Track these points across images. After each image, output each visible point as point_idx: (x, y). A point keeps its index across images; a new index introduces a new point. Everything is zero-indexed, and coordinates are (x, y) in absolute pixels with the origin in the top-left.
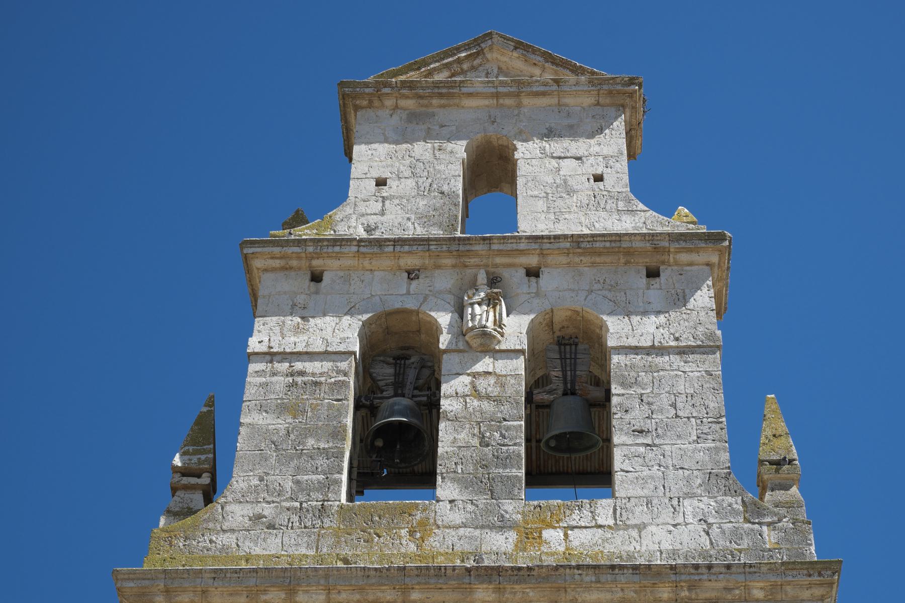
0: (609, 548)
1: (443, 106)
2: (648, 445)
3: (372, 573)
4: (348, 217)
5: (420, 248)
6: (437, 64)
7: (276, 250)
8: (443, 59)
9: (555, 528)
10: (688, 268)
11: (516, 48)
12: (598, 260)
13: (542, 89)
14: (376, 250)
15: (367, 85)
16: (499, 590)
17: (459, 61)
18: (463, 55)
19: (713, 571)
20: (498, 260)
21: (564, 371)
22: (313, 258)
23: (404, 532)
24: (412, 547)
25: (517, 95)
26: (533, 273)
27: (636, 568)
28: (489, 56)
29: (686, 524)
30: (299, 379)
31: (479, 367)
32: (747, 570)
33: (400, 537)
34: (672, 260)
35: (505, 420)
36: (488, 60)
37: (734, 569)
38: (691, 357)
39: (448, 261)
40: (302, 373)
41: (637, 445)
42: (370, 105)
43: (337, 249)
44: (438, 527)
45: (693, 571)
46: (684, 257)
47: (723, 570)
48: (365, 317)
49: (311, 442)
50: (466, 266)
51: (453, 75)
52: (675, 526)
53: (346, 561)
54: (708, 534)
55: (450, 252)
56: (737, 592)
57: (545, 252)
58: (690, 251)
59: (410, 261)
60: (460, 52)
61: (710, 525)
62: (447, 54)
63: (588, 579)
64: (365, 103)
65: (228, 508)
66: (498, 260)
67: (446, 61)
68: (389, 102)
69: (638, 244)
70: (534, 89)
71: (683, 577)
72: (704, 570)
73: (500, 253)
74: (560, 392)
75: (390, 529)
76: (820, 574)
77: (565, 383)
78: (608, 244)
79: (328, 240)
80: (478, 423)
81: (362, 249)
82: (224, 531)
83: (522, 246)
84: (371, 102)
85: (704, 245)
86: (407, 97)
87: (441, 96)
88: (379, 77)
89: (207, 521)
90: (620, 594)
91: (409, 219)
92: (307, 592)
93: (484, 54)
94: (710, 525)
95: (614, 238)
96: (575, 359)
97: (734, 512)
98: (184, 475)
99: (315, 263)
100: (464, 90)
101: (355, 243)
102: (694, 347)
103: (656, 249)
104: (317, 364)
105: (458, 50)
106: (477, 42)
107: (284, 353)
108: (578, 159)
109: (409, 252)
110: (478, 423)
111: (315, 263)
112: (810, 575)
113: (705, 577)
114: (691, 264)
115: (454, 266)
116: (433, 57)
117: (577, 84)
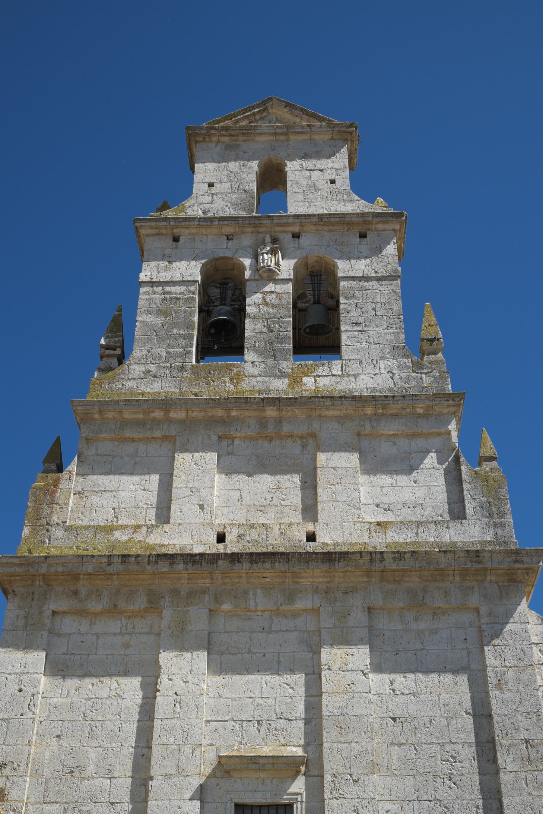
0: (339, 387)
1: (245, 141)
2: (360, 331)
3: (211, 401)
4: (193, 205)
5: (233, 222)
6: (241, 116)
7: (154, 224)
8: (245, 113)
9: (309, 376)
10: (382, 232)
11: (286, 106)
12: (332, 228)
13: (301, 130)
14: (209, 223)
15: (202, 129)
16: (279, 410)
17: (254, 114)
18: (256, 110)
19: (395, 399)
20: (277, 229)
21: (314, 290)
22: (173, 228)
23: (227, 379)
24: (232, 387)
25: (287, 134)
26: (296, 236)
27: (353, 397)
28: (270, 111)
29: (381, 374)
30: (168, 296)
31: (267, 289)
32: (414, 398)
33: (225, 382)
34: (373, 228)
35: (281, 318)
36: (270, 114)
37: (406, 398)
38: (384, 282)
39: (249, 230)
40: (169, 293)
41: (354, 331)
42: (204, 141)
43: (187, 223)
44: (246, 376)
45: (384, 399)
46: (381, 226)
47: (401, 398)
48: (204, 261)
49: (175, 331)
50: (259, 232)
51: (250, 123)
52: (375, 375)
53: (196, 395)
54: (392, 379)
55: (250, 224)
56: (408, 410)
57: (303, 224)
58: (384, 222)
59: (229, 230)
60: (254, 109)
61: (394, 374)
62: (247, 110)
63: (327, 404)
64: (201, 139)
65: (131, 367)
66: (277, 229)
67: (246, 114)
68: (214, 139)
69: (355, 219)
70: (296, 130)
71: (379, 402)
72: (391, 398)
73: (278, 225)
74: (312, 302)
75: (220, 378)
76: (453, 400)
77: (314, 297)
78: (338, 219)
79: (182, 218)
80: (267, 320)
81: (201, 223)
82: (130, 379)
83: (290, 221)
84: (204, 138)
85: (391, 219)
86: (225, 136)
87: (244, 134)
88: (208, 124)
89: (121, 374)
90: (345, 412)
91: (227, 206)
92: (175, 411)
93: (268, 110)
94: (394, 374)
95: (341, 216)
96: (320, 284)
97: (407, 367)
98: (107, 349)
99: (175, 231)
100: (257, 131)
101: (197, 220)
102: (385, 276)
103: (365, 222)
104: (178, 288)
105: (253, 107)
106: (264, 103)
107: (159, 282)
108: (321, 170)
109: (227, 225)
110: (267, 320)
111: (175, 231)
112: (448, 401)
113: (391, 402)
114: (384, 230)
115: (252, 232)
116: (239, 112)
117: (321, 127)
